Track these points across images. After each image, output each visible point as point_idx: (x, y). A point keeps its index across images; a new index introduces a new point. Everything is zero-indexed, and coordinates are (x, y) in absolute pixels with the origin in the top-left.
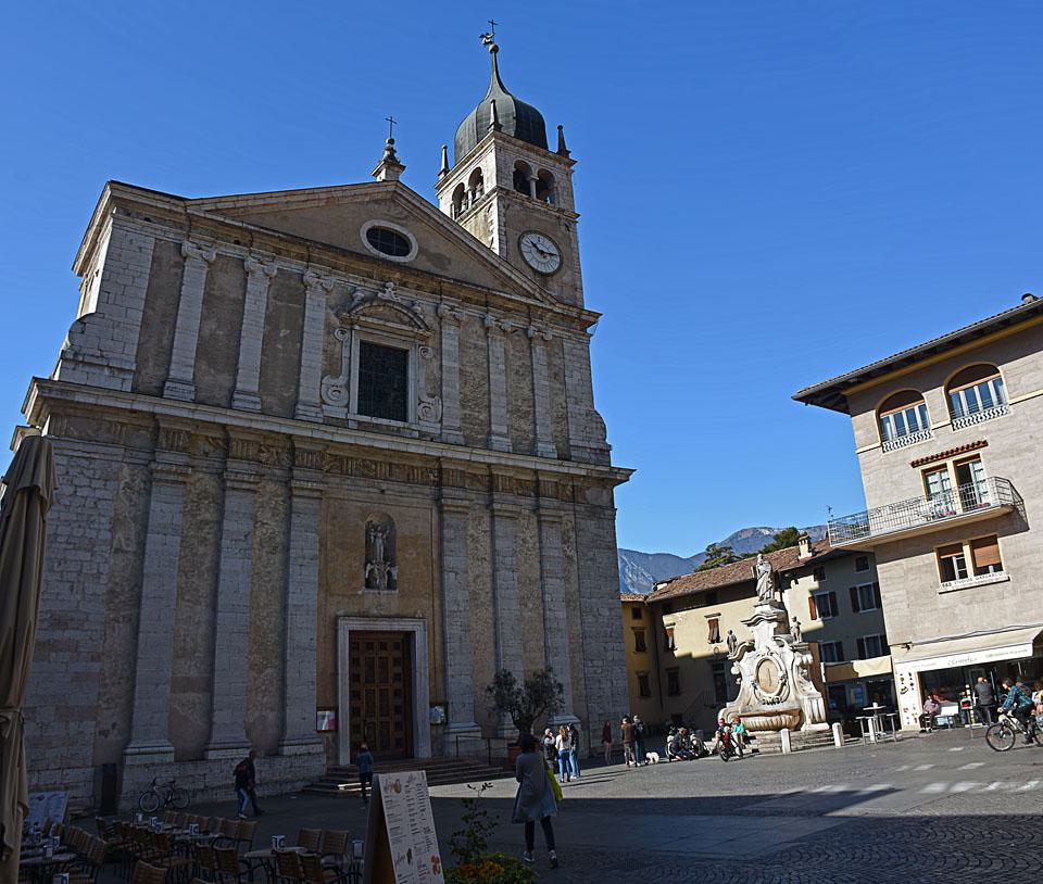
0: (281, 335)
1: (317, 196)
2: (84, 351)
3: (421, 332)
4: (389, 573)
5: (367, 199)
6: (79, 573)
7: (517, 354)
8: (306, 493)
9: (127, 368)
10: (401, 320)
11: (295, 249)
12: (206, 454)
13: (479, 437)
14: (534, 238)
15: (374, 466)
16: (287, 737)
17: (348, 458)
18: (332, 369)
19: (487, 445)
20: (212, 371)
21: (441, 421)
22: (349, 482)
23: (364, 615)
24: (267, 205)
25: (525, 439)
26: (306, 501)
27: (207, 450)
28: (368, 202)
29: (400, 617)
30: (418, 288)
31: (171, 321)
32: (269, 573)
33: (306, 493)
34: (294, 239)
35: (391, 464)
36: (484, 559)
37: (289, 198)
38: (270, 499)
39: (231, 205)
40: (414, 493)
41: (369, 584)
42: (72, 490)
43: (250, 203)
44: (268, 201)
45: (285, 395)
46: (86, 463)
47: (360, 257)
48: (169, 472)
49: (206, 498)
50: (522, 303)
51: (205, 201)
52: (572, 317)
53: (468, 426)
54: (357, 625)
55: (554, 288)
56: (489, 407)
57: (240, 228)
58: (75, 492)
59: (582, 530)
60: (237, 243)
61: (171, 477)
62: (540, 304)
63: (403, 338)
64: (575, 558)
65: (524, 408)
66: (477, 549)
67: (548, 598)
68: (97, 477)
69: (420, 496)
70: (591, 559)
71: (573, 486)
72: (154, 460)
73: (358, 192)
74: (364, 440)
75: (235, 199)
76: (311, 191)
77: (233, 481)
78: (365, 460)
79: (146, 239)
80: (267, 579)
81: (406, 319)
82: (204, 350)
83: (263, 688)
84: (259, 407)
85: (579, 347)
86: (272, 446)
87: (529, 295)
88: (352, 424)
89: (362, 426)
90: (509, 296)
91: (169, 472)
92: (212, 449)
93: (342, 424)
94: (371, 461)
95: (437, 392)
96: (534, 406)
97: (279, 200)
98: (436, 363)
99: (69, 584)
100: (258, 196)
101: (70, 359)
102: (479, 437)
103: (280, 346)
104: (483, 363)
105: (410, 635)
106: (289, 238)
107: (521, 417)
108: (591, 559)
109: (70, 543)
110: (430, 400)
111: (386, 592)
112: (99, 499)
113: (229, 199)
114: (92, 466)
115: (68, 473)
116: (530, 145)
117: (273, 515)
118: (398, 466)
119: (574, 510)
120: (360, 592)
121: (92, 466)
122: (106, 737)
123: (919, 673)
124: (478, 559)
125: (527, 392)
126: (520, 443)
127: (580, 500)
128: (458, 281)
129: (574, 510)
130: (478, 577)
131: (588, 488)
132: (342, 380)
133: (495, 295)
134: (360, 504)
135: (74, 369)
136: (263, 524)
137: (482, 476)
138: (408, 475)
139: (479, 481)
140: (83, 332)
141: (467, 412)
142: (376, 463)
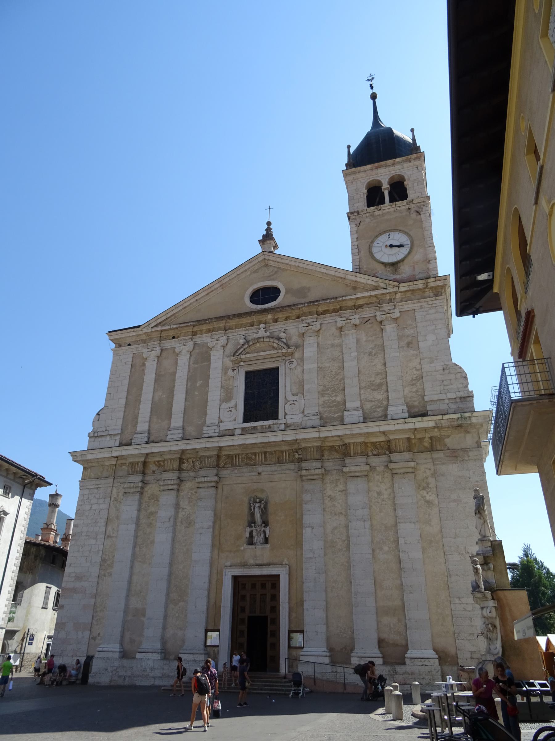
0: (198, 385)
1: (213, 288)
2: (99, 430)
3: (284, 351)
4: (265, 533)
5: (249, 273)
6: (90, 551)
7: (370, 338)
8: (206, 485)
9: (117, 433)
10: (273, 347)
11: (204, 327)
12: (154, 472)
13: (336, 415)
14: (384, 240)
15: (254, 457)
16: (184, 647)
17: (236, 455)
18: (228, 396)
19: (342, 422)
20: (160, 421)
21: (303, 412)
22: (236, 471)
23: (244, 565)
24: (185, 307)
25: (379, 407)
26: (206, 490)
27: (154, 469)
28: (250, 275)
29: (269, 564)
30: (287, 318)
31: (138, 400)
32: (185, 540)
33: (206, 485)
34: (200, 322)
35: (265, 453)
36: (341, 513)
37: (197, 298)
38: (188, 492)
39: (165, 318)
40: (283, 470)
41: (251, 542)
42: (89, 507)
43: (175, 311)
44: (185, 305)
45: (200, 423)
46: (96, 491)
47: (249, 314)
48: (130, 488)
49: (153, 499)
50: (371, 296)
51: (150, 322)
52: (420, 289)
53: (327, 409)
54: (238, 572)
55: (406, 270)
56: (344, 389)
57: (171, 329)
58: (91, 507)
59: (443, 475)
60: (174, 338)
61: (132, 490)
62: (385, 291)
63: (274, 360)
64: (436, 502)
65: (378, 381)
66: (334, 506)
67: (401, 541)
68: (101, 497)
69: (287, 472)
70: (455, 501)
71: (431, 438)
72: (390, 462)
73: (239, 272)
74: (251, 439)
75: (165, 313)
76: (208, 287)
77: (163, 485)
78: (247, 454)
79: (127, 354)
80: (184, 544)
81: (276, 345)
82: (155, 410)
83: (177, 615)
84: (181, 435)
85: (433, 311)
86: (190, 458)
87: (376, 288)
88: (238, 432)
89: (245, 431)
90: (354, 297)
91: (130, 488)
92: (157, 468)
93: (231, 433)
94: (251, 453)
95: (301, 391)
96: (386, 378)
97: (191, 301)
98: (299, 369)
99: (86, 558)
100: (177, 306)
101: (93, 436)
102: (336, 415)
103: (196, 393)
104: (339, 356)
105: (278, 576)
106: (196, 323)
107: (374, 390)
108: (455, 501)
109: (87, 536)
110: (295, 398)
111: (260, 547)
112: (101, 509)
113: (162, 315)
114: (99, 492)
115: (89, 498)
116: (376, 164)
117: (189, 502)
118: (271, 453)
119: (432, 458)
120: (242, 548)
121: (99, 492)
122: (95, 641)
123: (279, 576)
124: (335, 514)
125: (380, 367)
126: (375, 411)
127: (439, 448)
128: (311, 302)
129: (432, 458)
130: (335, 528)
131: (448, 437)
132: (232, 403)
133: (343, 300)
134: (244, 485)
135: (94, 441)
136: (183, 509)
137: (339, 446)
138: (278, 458)
139: (336, 451)
140: (98, 420)
141: (326, 398)
142: (255, 454)
